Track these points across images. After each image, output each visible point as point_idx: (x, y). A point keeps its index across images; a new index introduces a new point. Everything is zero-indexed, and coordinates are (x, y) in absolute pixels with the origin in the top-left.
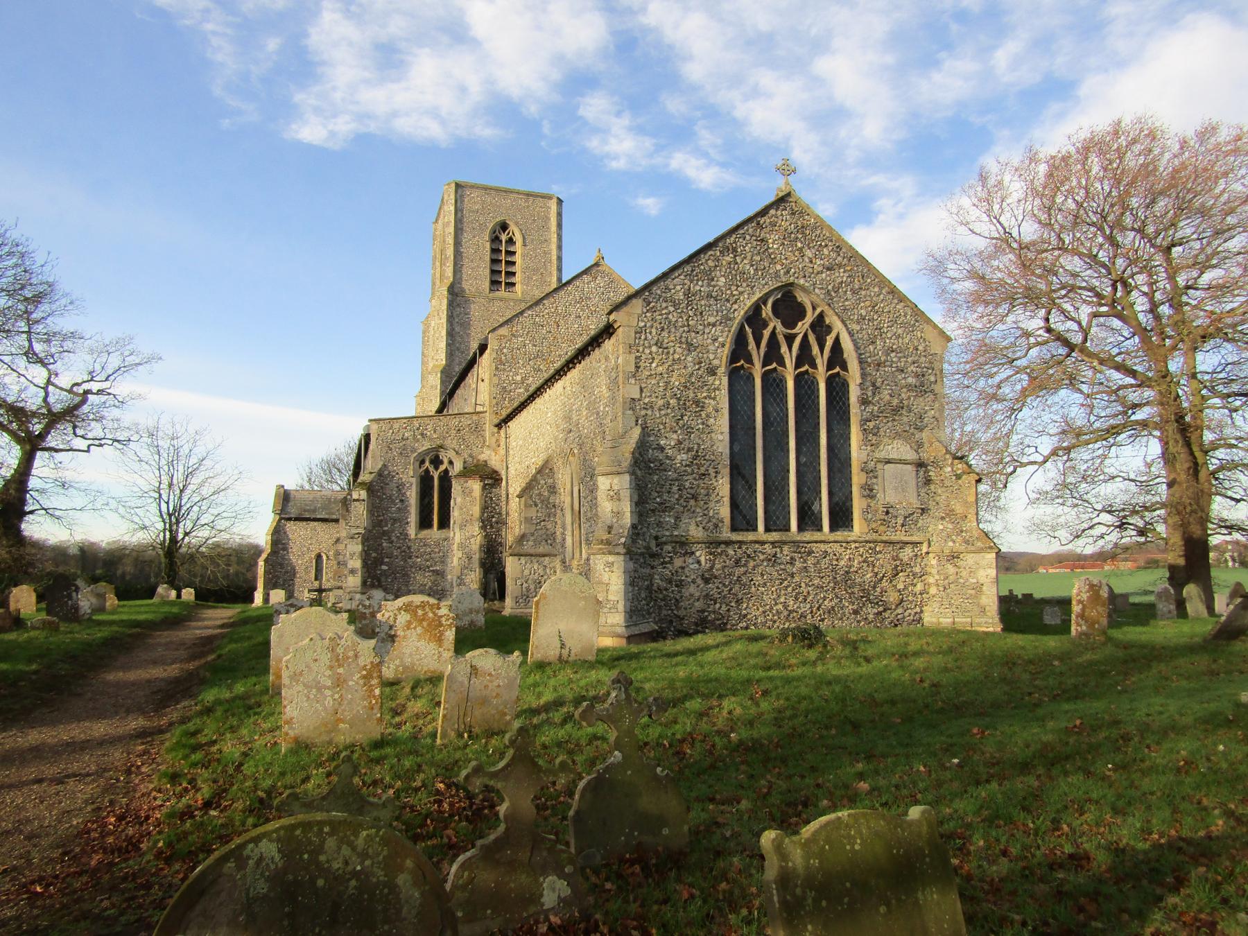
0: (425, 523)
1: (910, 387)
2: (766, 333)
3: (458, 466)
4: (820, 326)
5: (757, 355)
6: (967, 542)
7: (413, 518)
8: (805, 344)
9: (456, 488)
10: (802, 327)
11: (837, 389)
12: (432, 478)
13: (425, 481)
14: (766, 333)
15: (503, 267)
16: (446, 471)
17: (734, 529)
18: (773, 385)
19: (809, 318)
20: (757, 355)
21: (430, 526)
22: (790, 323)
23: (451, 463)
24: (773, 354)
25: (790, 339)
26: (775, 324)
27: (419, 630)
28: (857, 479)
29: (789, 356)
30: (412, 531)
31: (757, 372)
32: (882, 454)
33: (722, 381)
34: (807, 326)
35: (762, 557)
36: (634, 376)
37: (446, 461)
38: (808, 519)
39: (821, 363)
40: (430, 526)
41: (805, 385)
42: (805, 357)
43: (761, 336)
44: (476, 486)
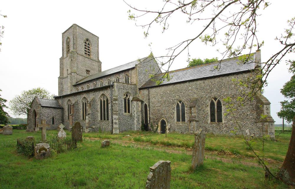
12: (105, 101)
16: (129, 98)
38: (105, 119)
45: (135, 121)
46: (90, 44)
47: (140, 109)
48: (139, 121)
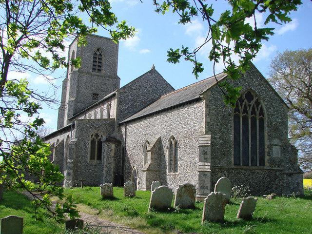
0: (92, 158)
1: (280, 123)
2: (244, 104)
3: (104, 138)
4: (257, 103)
5: (241, 109)
6: (295, 170)
7: (89, 156)
8: (253, 108)
9: (105, 146)
10: (253, 102)
11: (262, 121)
13: (93, 142)
14: (244, 104)
15: (97, 60)
17: (234, 165)
18: (245, 119)
19: (255, 99)
20: (241, 109)
21: (94, 159)
22: (249, 101)
23: (102, 136)
24: (245, 111)
25: (250, 106)
26: (246, 101)
27: (187, 193)
28: (267, 150)
29: (250, 110)
30: (88, 160)
31: (250, 116)
32: (272, 143)
33: (232, 118)
34: (254, 102)
35: (242, 174)
36: (208, 115)
37: (100, 135)
39: (258, 112)
40: (94, 159)
41: (254, 120)
42: (253, 112)
43: (242, 104)
44: (113, 146)
45: (104, 172)
46: (102, 54)
47: (112, 154)
48: (109, 171)
